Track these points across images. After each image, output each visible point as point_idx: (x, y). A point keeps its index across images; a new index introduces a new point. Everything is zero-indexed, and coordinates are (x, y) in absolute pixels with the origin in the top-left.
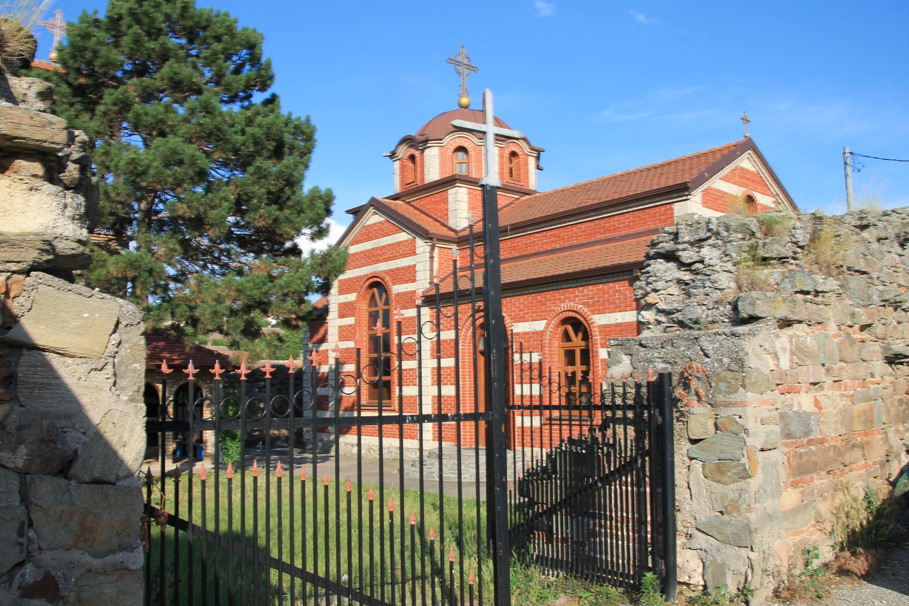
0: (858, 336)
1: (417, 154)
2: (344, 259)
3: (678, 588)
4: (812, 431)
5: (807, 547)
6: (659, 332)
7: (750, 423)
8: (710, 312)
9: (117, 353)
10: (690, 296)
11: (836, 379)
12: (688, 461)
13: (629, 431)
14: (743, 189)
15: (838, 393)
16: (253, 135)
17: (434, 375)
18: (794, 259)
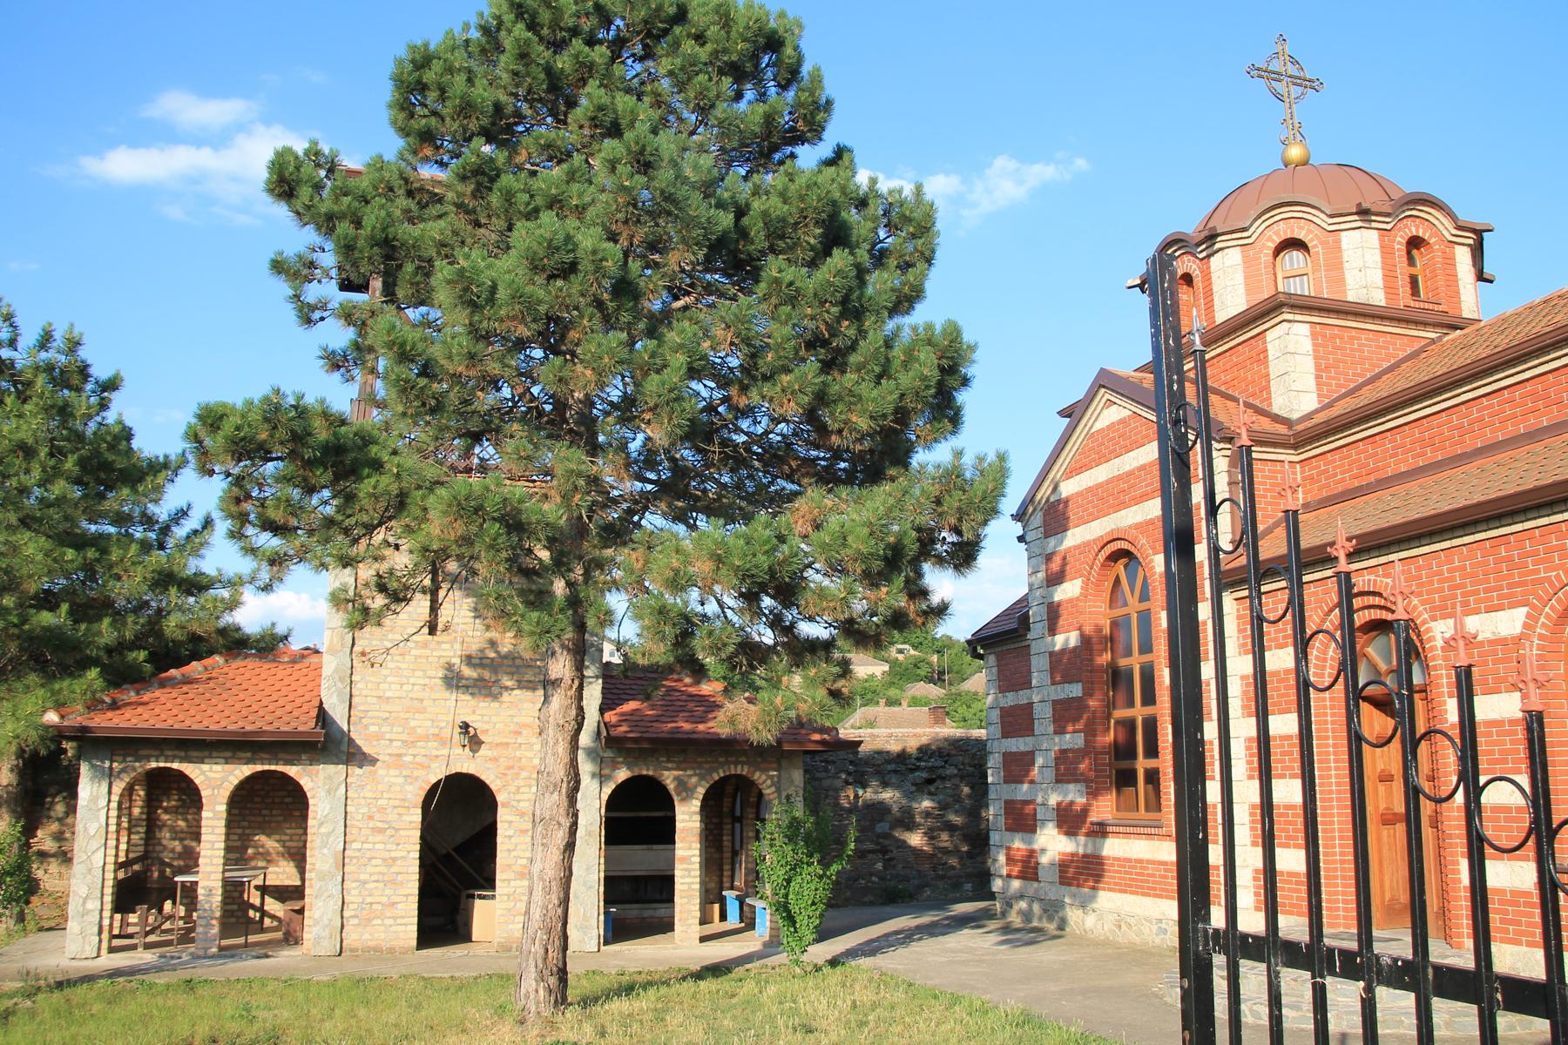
17: (1251, 755)
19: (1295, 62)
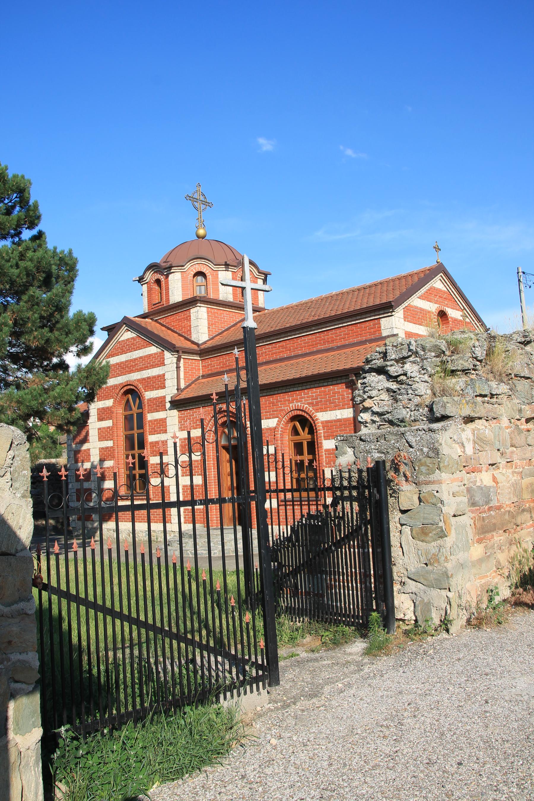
0: (524, 426)
1: (162, 278)
2: (107, 372)
3: (396, 624)
4: (491, 500)
5: (491, 588)
6: (374, 429)
7: (445, 496)
8: (412, 413)
9: (12, 464)
10: (397, 401)
11: (508, 460)
12: (400, 527)
13: (354, 507)
14: (436, 306)
15: (510, 471)
16: (26, 268)
18: (475, 370)
19: (203, 195)
